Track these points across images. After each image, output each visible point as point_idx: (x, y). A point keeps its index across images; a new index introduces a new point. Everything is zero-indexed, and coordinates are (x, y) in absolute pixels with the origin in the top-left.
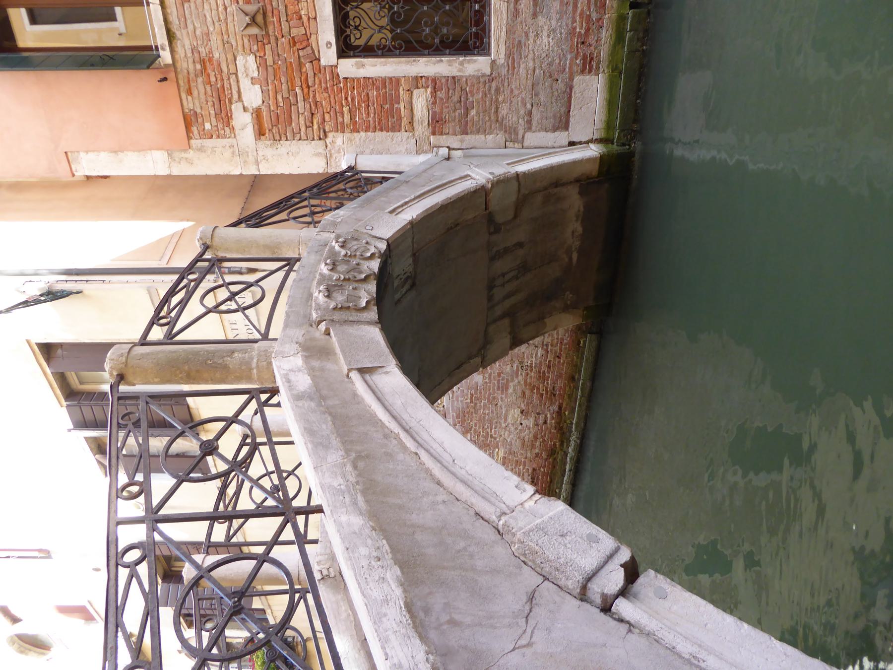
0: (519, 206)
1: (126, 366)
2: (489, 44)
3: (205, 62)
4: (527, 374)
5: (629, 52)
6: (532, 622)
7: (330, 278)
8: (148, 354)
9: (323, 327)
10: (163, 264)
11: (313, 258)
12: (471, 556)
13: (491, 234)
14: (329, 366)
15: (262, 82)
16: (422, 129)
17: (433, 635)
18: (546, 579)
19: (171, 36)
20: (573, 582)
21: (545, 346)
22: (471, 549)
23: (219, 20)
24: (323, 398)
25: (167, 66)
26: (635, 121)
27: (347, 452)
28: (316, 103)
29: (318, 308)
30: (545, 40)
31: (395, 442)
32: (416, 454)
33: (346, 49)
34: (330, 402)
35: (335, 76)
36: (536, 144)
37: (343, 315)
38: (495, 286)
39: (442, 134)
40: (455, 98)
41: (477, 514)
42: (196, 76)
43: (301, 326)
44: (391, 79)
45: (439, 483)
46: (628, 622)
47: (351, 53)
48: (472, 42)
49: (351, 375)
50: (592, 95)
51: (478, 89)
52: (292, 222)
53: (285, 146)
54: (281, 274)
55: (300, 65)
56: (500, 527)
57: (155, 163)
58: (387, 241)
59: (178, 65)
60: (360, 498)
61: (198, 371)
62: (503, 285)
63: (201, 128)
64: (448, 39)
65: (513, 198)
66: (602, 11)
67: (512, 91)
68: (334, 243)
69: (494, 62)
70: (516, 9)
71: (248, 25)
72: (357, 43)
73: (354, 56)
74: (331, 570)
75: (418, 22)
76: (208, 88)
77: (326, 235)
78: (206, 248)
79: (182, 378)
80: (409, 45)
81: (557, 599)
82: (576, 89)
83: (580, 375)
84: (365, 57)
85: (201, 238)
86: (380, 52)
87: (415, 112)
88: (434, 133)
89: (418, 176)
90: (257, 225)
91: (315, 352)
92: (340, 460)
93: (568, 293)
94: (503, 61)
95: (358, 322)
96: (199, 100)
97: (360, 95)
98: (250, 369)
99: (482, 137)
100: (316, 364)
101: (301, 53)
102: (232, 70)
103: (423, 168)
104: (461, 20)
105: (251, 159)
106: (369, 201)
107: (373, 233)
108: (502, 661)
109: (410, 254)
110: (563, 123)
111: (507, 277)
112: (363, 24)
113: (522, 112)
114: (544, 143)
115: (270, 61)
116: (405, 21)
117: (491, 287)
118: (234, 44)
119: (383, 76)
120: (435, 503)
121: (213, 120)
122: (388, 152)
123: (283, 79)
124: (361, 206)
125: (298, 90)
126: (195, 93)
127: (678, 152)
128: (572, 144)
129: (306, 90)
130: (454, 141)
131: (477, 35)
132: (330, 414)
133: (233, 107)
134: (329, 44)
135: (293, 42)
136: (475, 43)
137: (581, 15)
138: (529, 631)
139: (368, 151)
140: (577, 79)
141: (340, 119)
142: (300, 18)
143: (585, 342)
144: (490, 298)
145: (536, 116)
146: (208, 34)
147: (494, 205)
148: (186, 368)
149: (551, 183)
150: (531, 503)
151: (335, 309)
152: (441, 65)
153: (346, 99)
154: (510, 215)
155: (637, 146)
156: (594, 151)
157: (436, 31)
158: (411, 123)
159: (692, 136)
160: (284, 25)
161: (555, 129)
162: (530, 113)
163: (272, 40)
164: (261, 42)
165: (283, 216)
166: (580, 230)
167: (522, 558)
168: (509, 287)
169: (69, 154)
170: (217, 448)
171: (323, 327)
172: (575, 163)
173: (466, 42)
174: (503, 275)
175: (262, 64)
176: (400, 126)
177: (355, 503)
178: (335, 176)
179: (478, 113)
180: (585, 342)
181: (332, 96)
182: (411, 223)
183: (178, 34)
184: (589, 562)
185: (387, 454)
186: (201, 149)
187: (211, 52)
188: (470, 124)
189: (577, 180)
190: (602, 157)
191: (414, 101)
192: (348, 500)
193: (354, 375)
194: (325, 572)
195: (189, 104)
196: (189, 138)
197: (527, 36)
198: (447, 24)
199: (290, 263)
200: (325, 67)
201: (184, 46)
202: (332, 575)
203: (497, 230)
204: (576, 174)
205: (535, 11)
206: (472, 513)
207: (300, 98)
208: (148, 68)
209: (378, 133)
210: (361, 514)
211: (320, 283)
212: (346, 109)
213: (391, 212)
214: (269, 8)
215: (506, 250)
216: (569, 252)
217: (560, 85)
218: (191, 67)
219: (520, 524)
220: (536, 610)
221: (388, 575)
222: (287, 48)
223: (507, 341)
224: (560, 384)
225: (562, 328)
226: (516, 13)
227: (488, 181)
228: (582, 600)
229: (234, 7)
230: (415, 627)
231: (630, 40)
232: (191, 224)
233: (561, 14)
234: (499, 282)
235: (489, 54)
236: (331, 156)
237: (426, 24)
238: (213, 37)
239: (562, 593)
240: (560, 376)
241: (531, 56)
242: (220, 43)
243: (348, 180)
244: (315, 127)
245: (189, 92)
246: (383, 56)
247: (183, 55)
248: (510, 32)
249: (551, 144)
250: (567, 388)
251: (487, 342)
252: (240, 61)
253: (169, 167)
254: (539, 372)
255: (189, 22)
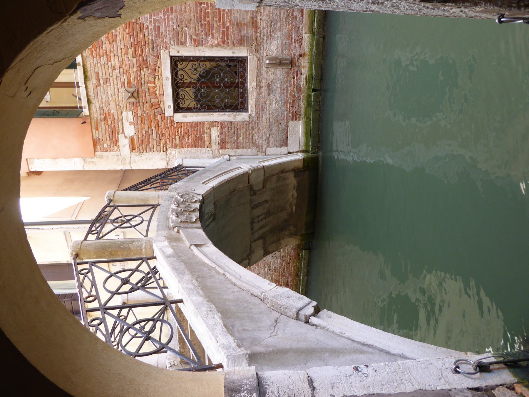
0: (266, 181)
1: (80, 249)
2: (248, 107)
3: (106, 115)
4: (273, 274)
5: (314, 111)
6: (277, 328)
7: (177, 210)
8: (91, 244)
9: (176, 229)
10: (73, 219)
11: (167, 203)
12: (251, 309)
13: (251, 195)
14: (180, 245)
15: (135, 124)
16: (215, 146)
17: (236, 334)
18: (282, 314)
19: (89, 102)
20: (293, 314)
21: (281, 257)
22: (251, 306)
23: (115, 95)
24: (180, 257)
25: (86, 116)
26: (319, 142)
27: (193, 276)
28: (162, 134)
29: (173, 222)
30: (274, 105)
31: (214, 271)
32: (224, 274)
33: (178, 109)
34: (183, 258)
35: (172, 121)
36: (272, 153)
37: (185, 225)
38: (254, 222)
39: (225, 149)
40: (232, 132)
41: (252, 294)
42: (101, 121)
43: (165, 230)
44: (200, 123)
45: (235, 285)
46: (316, 325)
47: (181, 111)
48: (239, 105)
49: (191, 247)
50: (298, 131)
51: (243, 127)
52: (153, 189)
53: (145, 155)
54: (152, 210)
55: (155, 116)
56: (262, 298)
57: (76, 164)
58: (202, 195)
59: (92, 116)
60: (201, 291)
61: (115, 251)
62: (258, 222)
63: (101, 146)
64: (228, 104)
65: (262, 178)
66: (300, 93)
67: (259, 128)
68: (177, 196)
69: (250, 115)
70: (260, 92)
71: (129, 97)
72: (183, 106)
73: (182, 112)
74: (175, 362)
75: (213, 97)
76: (107, 127)
77: (172, 193)
78: (111, 201)
79: (107, 255)
80: (210, 108)
81: (287, 320)
82: (290, 128)
83: (301, 273)
84: (187, 112)
85: (108, 197)
86: (195, 110)
87: (212, 138)
88: (221, 148)
89: (215, 167)
90: (136, 190)
91: (173, 240)
92: (190, 278)
93: (291, 227)
94: (254, 115)
95: (192, 228)
96: (102, 133)
97: (184, 130)
98: (142, 249)
99: (246, 150)
100: (174, 244)
101: (156, 111)
102: (120, 118)
103: (217, 164)
104: (234, 96)
105: (127, 161)
106: (192, 179)
107: (195, 192)
108: (265, 341)
109: (213, 203)
110: (284, 143)
111: (261, 218)
112: (186, 97)
113: (265, 138)
114: (276, 153)
115: (139, 114)
116: (207, 96)
117: (252, 223)
118: (122, 106)
119: (196, 121)
120: (233, 292)
121: (109, 142)
122: (198, 157)
123: (146, 123)
124: (188, 181)
125: (153, 128)
126: (100, 129)
127: (343, 157)
128: (289, 153)
129: (157, 128)
130: (232, 152)
131: (241, 103)
132: (183, 262)
133: (119, 136)
134: (170, 106)
135: (152, 105)
136: (241, 106)
137: (290, 94)
138: (276, 331)
139: (188, 157)
140: (291, 123)
141: (174, 142)
142: (156, 94)
143: (302, 254)
144: (252, 229)
145: (272, 140)
146: (108, 101)
147: (252, 181)
148: (110, 250)
149: (279, 172)
150: (275, 289)
151: (181, 222)
152: (225, 116)
153: (178, 132)
154: (260, 187)
155: (320, 154)
156: (300, 156)
157: (222, 101)
158: (210, 143)
159: (346, 148)
160: (148, 97)
161: (281, 146)
162: (269, 139)
163: (141, 104)
164: (135, 105)
165: (148, 186)
166: (296, 194)
167: (272, 308)
168: (262, 223)
169: (28, 160)
170: (129, 281)
171: (176, 229)
172: (291, 162)
173: (236, 106)
174: (258, 217)
175: (135, 115)
176: (205, 145)
177: (199, 293)
178: (172, 169)
179: (243, 139)
180: (302, 254)
181: (170, 131)
182: (213, 188)
183: (93, 101)
184: (300, 305)
185: (211, 276)
186: (101, 157)
187: (109, 110)
188: (239, 144)
189: (293, 170)
190: (304, 159)
191: (211, 133)
192: (195, 292)
193: (193, 247)
194: (172, 363)
195: (96, 134)
196: (95, 151)
197: (265, 103)
198: (228, 98)
199: (154, 207)
200: (167, 117)
201: (96, 107)
202: (176, 364)
203: (255, 194)
204: (292, 167)
205: (269, 92)
206: (250, 294)
207: (154, 131)
208: (77, 117)
209: (194, 149)
210: (201, 296)
211: (172, 212)
212: (177, 137)
213: (203, 183)
214: (140, 90)
215: (260, 204)
216: (291, 205)
217: (282, 126)
218: (99, 117)
219: (270, 295)
220: (278, 324)
221: (216, 316)
222: (148, 108)
223: (261, 252)
224: (290, 279)
225: (289, 246)
226: (260, 93)
227: (249, 169)
228: (297, 320)
229: (123, 89)
230: (228, 332)
231: (314, 105)
232: (88, 198)
233: (281, 94)
234: (256, 220)
235: (248, 112)
236: (169, 160)
237: (217, 98)
238: (111, 103)
239: (289, 319)
240: (290, 274)
241: (268, 112)
242: (114, 105)
243: (179, 171)
244: (162, 145)
245: (97, 129)
246: (196, 112)
247: (95, 111)
248: (257, 101)
249: (279, 153)
250: (295, 281)
251: (251, 252)
252: (124, 114)
253: (83, 166)
254: (279, 272)
255: (99, 95)
